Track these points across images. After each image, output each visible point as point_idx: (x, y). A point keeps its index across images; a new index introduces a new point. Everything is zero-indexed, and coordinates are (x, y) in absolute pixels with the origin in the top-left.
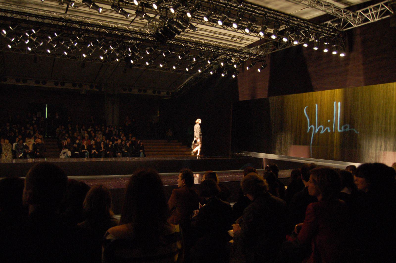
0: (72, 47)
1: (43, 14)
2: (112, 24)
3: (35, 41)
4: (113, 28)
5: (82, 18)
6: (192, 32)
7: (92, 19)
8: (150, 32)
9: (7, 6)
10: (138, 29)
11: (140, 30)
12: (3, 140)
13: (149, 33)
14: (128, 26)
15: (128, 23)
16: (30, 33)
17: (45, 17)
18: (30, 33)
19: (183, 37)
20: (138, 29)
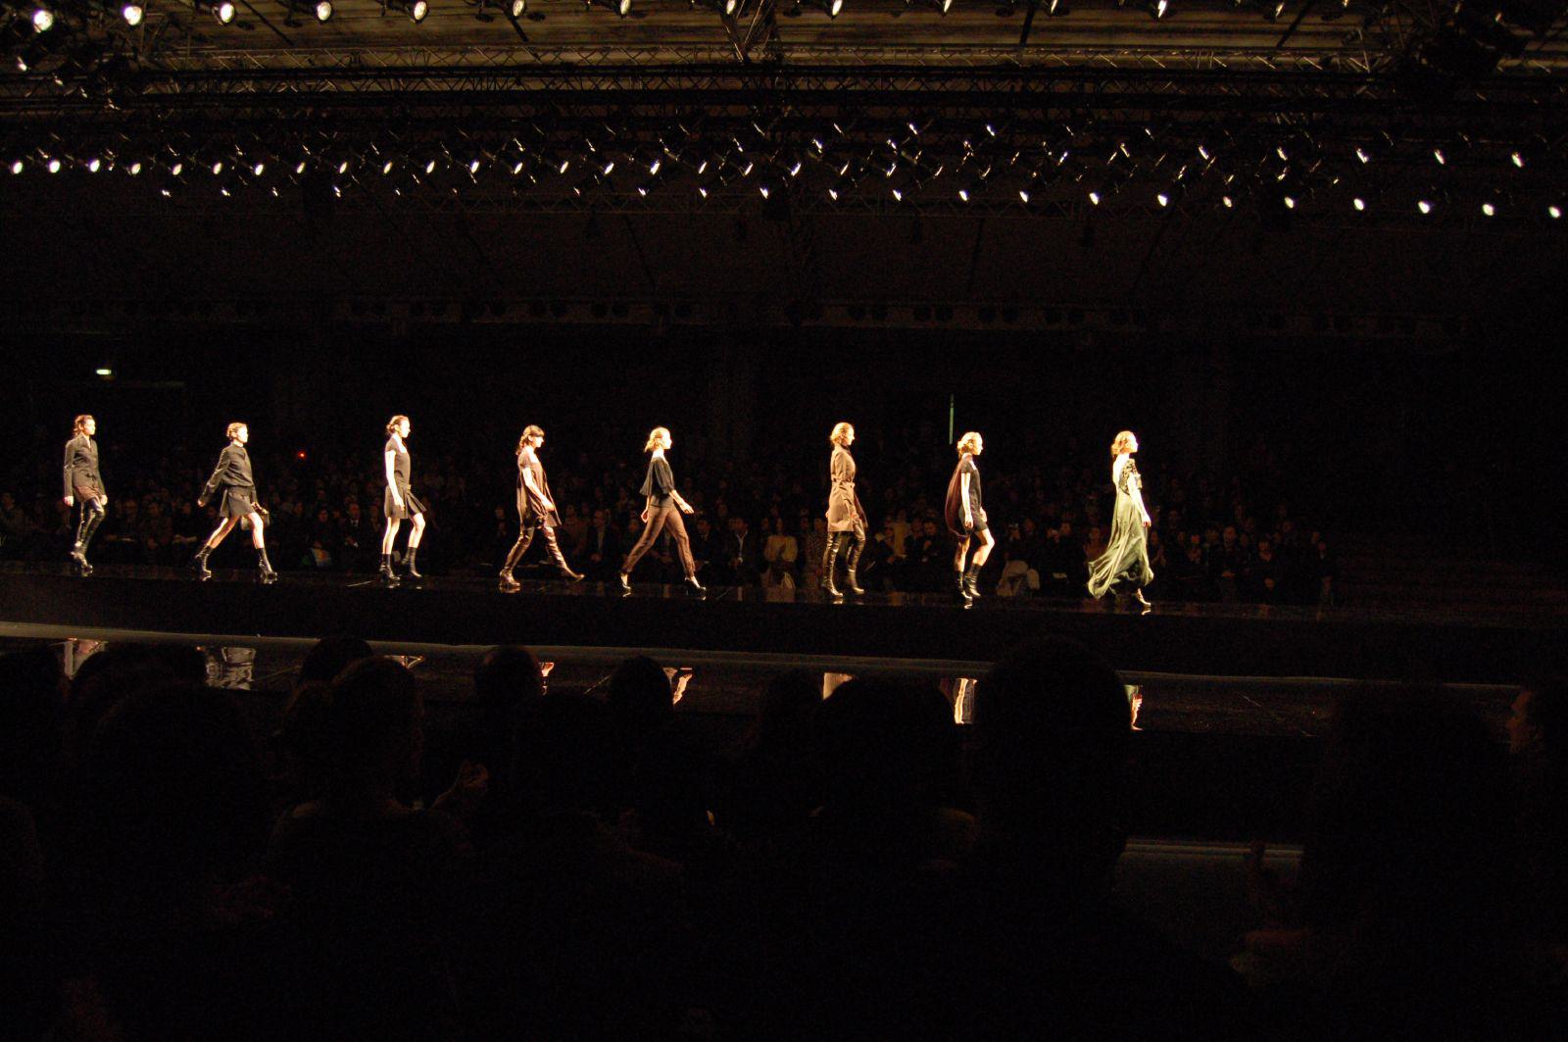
0: (1050, 171)
1: (1087, 62)
2: (1204, 58)
3: (915, 162)
4: (1211, 72)
5: (1084, 49)
6: (1257, 27)
7: (1122, 50)
8: (1372, 62)
9: (825, 54)
10: (1318, 59)
11: (1325, 62)
12: (355, 509)
13: (1367, 68)
14: (1269, 53)
15: (1271, 42)
16: (901, 134)
17: (951, 68)
18: (901, 134)
19: (1534, 63)
20: (1318, 59)
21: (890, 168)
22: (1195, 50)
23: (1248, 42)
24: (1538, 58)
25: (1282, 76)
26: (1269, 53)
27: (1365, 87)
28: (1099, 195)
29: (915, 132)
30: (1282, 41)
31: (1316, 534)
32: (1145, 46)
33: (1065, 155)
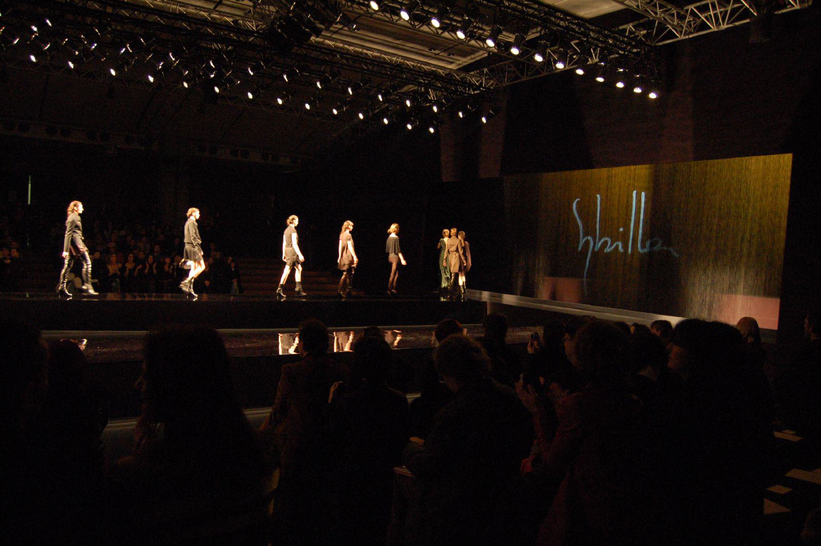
0: (86, 52)
1: (163, 7)
2: (174, 7)
4: (177, 15)
6: (443, 58)
8: (257, 27)
10: (232, 19)
11: (235, 22)
24: (329, 40)
25: (213, 24)
27: (253, 38)
28: (115, 70)
31: (230, 258)
33: (4, 28)
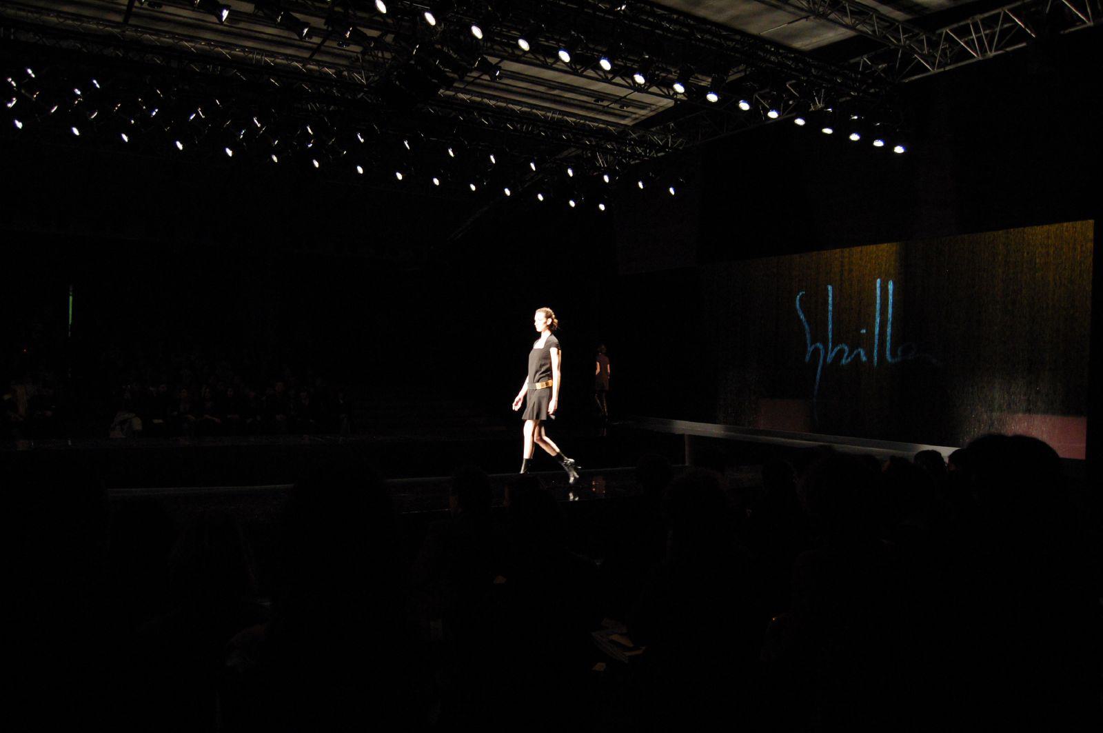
2: (259, 57)
10: (334, 71)
11: (339, 73)
14: (304, 61)
16: (21, 77)
18: (21, 77)
20: (334, 71)
21: (11, 101)
22: (252, 50)
23: (250, 44)
25: (310, 77)
26: (304, 61)
29: (33, 76)
30: (482, 75)
32: (182, 35)
